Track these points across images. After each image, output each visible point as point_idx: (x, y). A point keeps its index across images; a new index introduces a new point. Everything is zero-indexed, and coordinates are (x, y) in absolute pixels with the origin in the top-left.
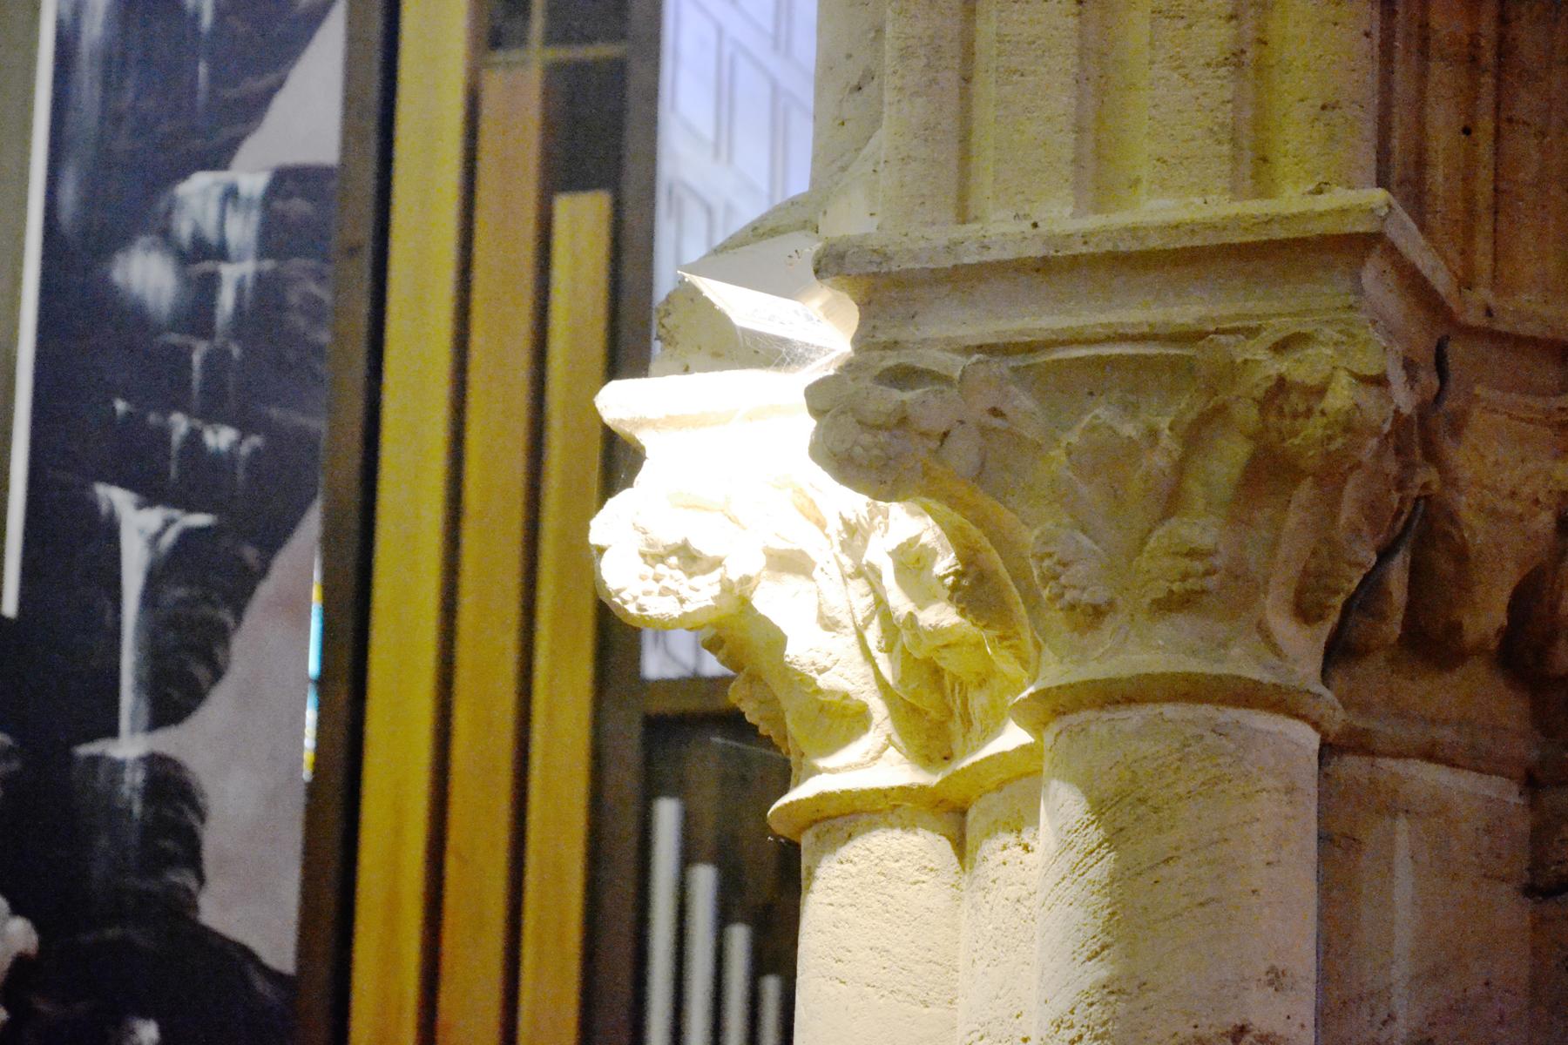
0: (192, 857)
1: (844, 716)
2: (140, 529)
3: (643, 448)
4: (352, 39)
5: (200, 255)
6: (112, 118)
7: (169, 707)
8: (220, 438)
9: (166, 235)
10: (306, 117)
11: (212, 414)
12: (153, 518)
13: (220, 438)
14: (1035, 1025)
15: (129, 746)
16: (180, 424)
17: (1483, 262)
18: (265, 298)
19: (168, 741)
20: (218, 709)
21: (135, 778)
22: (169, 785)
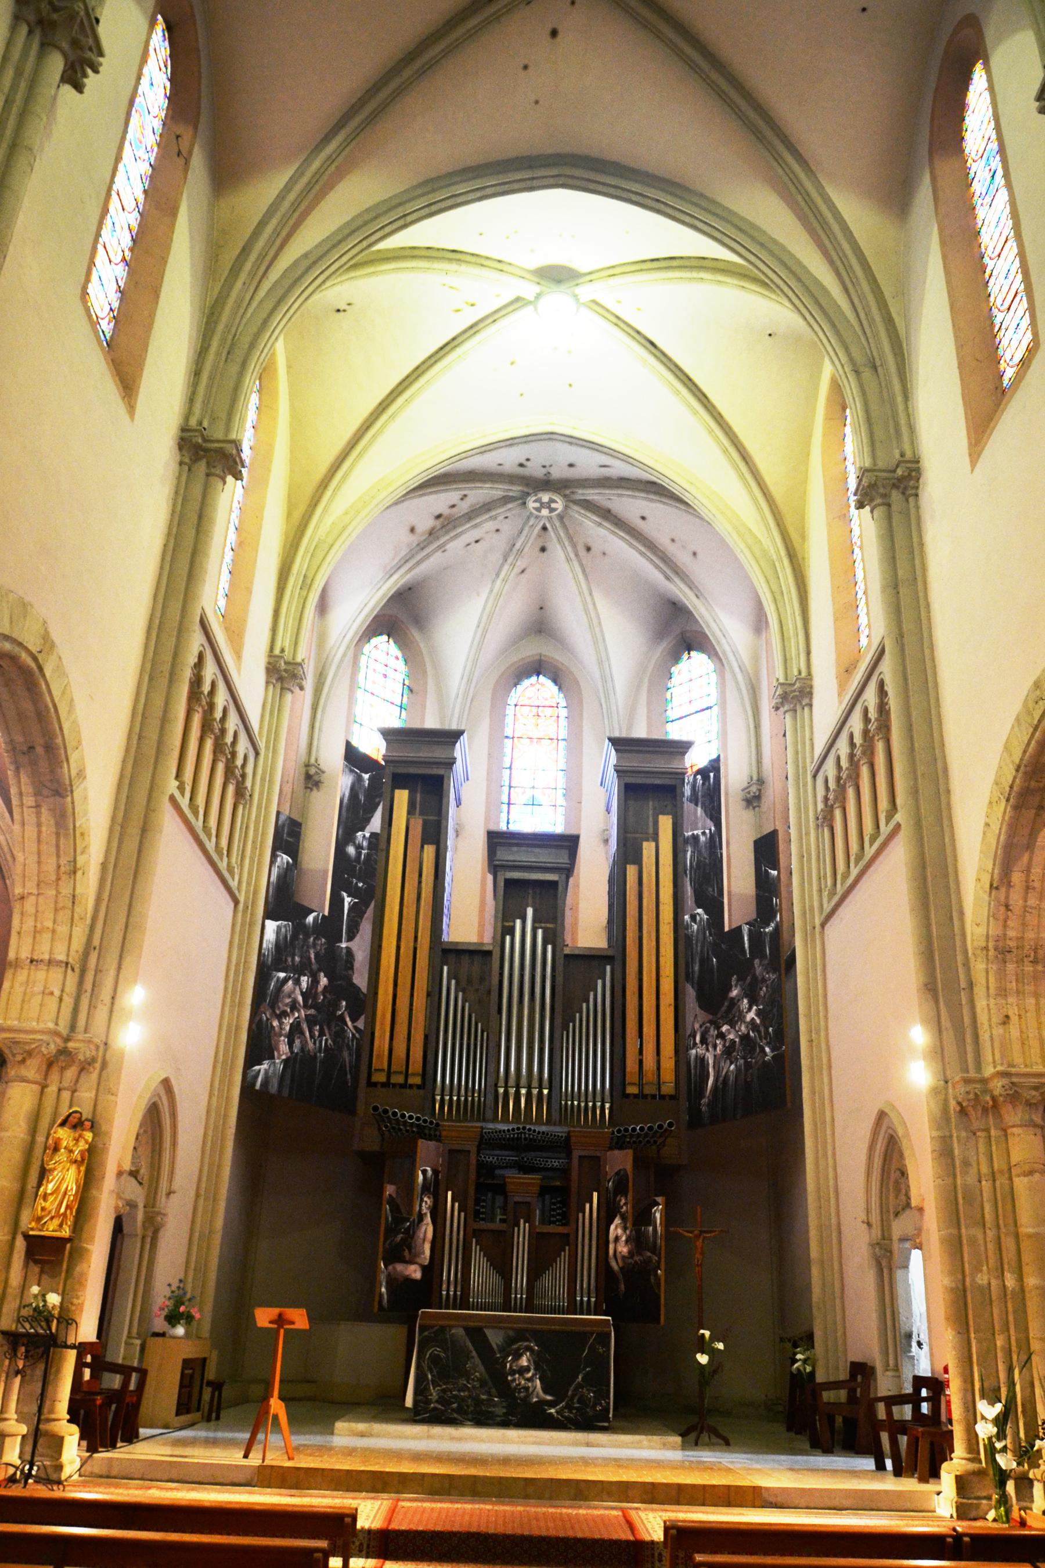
0: (352, 968)
1: (12, 741)
2: (347, 900)
3: (947, 1319)
4: (383, 813)
5: (359, 848)
6: (347, 818)
7: (350, 939)
8: (360, 885)
9: (354, 843)
10: (376, 824)
11: (359, 880)
12: (349, 899)
13: (360, 885)
14: (107, 4)
15: (344, 945)
16: (355, 881)
17: (215, 1168)
18: (368, 855)
19: (349, 944)
20: (357, 939)
21: (344, 951)
22: (349, 950)
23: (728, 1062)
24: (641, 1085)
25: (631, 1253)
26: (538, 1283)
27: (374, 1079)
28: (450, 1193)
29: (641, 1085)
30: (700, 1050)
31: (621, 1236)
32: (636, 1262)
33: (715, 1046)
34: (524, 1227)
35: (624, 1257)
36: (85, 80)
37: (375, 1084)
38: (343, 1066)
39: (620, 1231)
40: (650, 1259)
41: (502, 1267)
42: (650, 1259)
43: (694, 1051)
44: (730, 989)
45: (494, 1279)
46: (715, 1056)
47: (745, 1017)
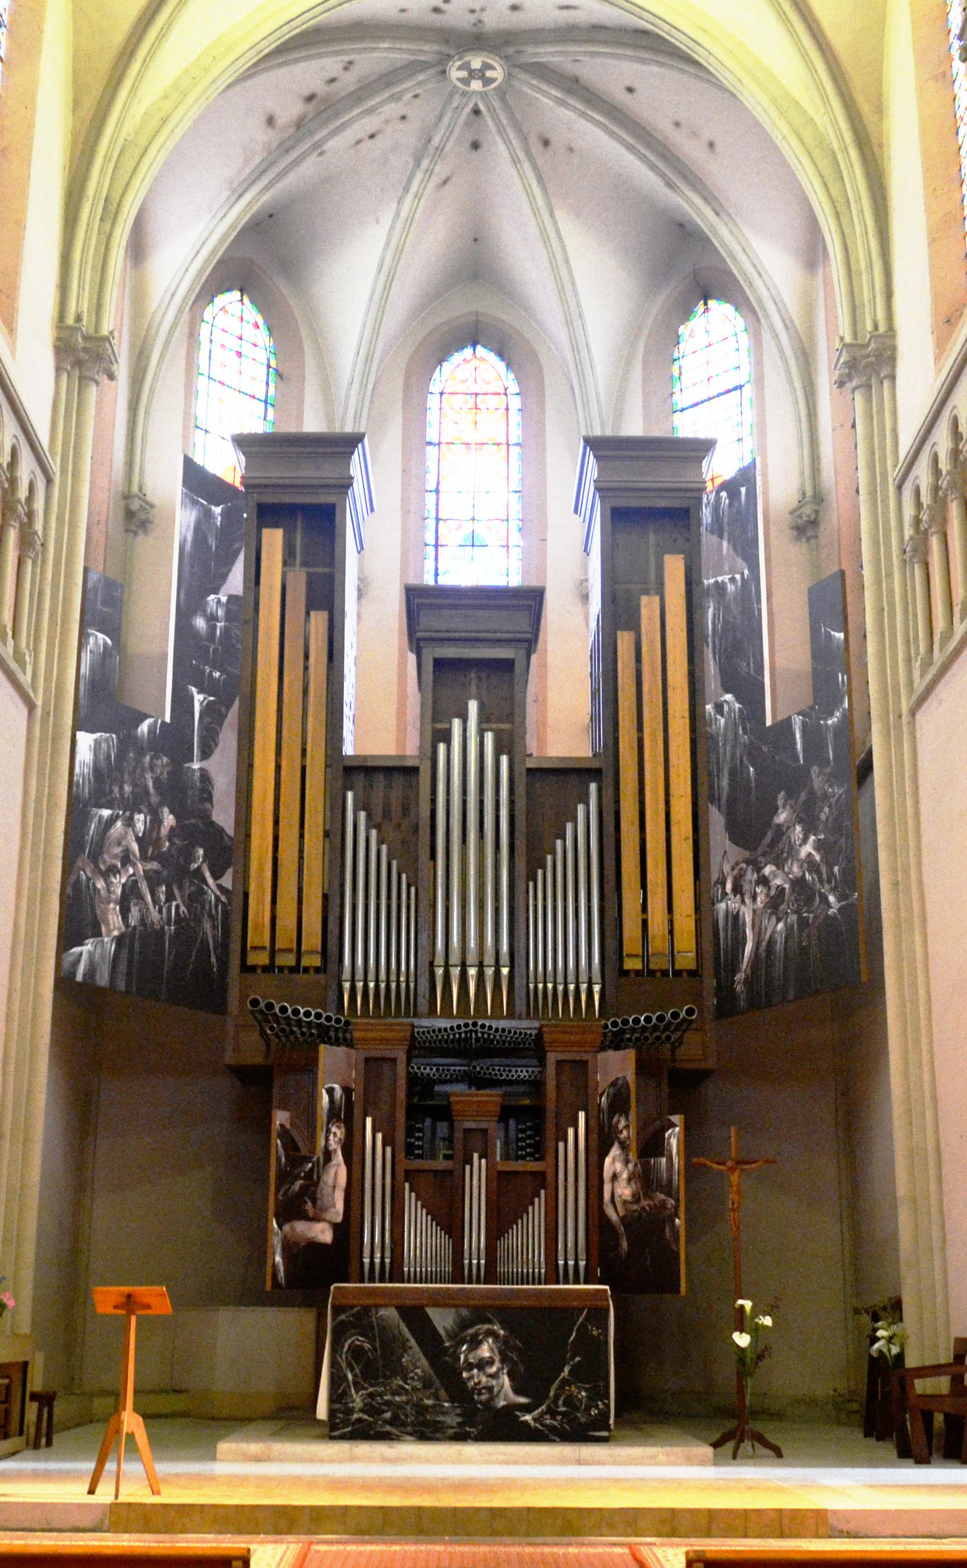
25: (636, 1198)
30: (733, 903)
33: (754, 897)
37: (253, 969)
39: (619, 1166)
40: (663, 1204)
41: (450, 1221)
42: (663, 1204)
46: (754, 911)
47: (798, 852)
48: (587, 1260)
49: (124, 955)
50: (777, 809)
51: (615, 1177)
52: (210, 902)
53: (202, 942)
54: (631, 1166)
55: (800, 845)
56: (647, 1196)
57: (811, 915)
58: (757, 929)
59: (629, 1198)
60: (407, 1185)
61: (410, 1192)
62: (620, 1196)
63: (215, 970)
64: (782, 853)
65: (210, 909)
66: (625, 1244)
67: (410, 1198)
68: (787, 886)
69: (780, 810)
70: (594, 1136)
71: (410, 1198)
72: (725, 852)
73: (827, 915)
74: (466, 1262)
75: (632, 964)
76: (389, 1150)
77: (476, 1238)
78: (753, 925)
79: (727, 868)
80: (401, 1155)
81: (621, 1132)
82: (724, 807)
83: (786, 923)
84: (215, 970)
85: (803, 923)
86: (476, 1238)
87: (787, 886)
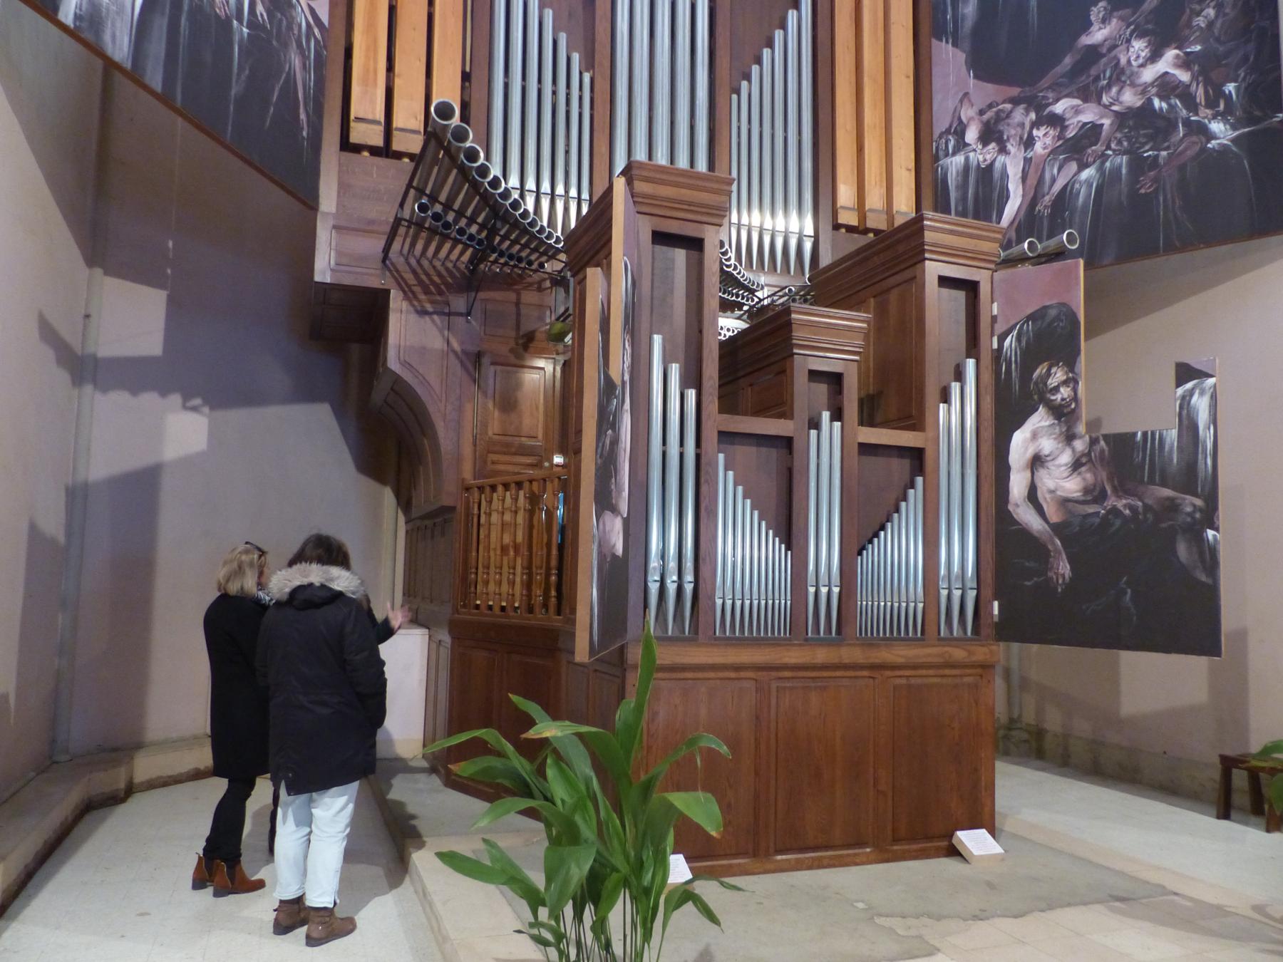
13: (169, 271)
23: (1074, 166)
24: (862, 215)
25: (1094, 494)
26: (873, 554)
27: (354, 138)
28: (657, 339)
29: (862, 215)
30: (982, 155)
31: (1053, 456)
32: (1114, 511)
33: (1029, 143)
34: (831, 431)
35: (1065, 502)
36: (210, 890)
37: (357, 149)
38: (290, 80)
39: (1047, 445)
40: (1172, 507)
41: (787, 525)
42: (1172, 507)
43: (959, 159)
44: (1086, 26)
45: (772, 549)
46: (1027, 161)
47: (1137, 75)
48: (978, 589)
49: (160, 25)
50: (1091, 24)
51: (1037, 462)
52: (300, 26)
53: (287, 81)
54: (1080, 445)
55: (1142, 66)
56: (1121, 490)
57: (1164, 153)
58: (1032, 180)
59: (1077, 495)
60: (721, 456)
61: (726, 469)
62: (1052, 492)
63: (305, 134)
64: (1097, 78)
65: (300, 36)
66: (1064, 568)
67: (726, 483)
68: (1106, 122)
69: (1095, 27)
70: (988, 401)
71: (726, 483)
72: (966, 94)
73: (1204, 150)
74: (812, 590)
75: (844, 218)
76: (691, 394)
77: (825, 548)
78: (1024, 178)
79: (967, 113)
80: (712, 404)
81: (1056, 390)
82: (967, 44)
83: (1101, 169)
84: (305, 134)
85: (1139, 165)
86: (825, 548)
87: (1106, 122)
